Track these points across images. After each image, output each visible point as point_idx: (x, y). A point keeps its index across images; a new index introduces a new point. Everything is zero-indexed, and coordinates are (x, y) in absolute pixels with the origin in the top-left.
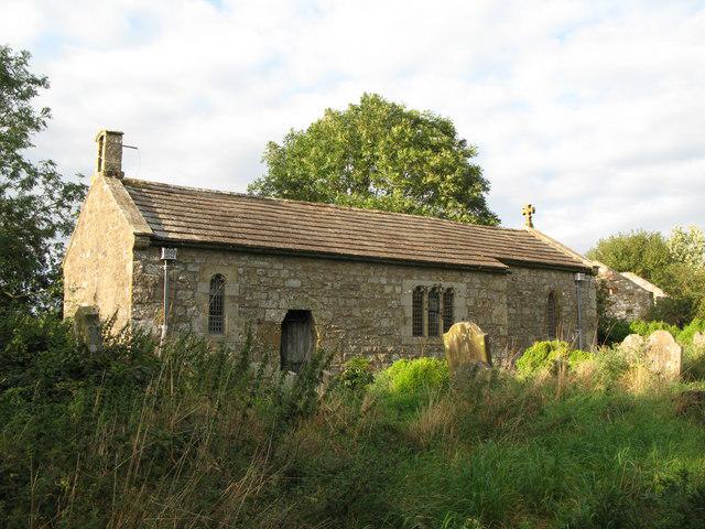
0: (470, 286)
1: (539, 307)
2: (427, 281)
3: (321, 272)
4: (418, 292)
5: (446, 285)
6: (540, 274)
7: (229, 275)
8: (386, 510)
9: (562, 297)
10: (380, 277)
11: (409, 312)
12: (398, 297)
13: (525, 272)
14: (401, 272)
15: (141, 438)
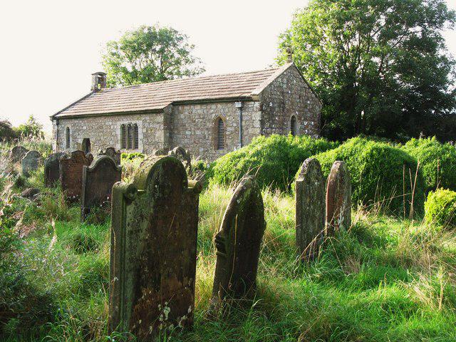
0: (144, 121)
1: (207, 129)
2: (126, 121)
3: (94, 123)
4: (123, 127)
5: (133, 122)
6: (209, 107)
7: (140, 123)
8: (388, 283)
9: (226, 121)
10: (109, 122)
11: (119, 137)
12: (114, 130)
13: (198, 107)
14: (116, 118)
15: (407, 181)
